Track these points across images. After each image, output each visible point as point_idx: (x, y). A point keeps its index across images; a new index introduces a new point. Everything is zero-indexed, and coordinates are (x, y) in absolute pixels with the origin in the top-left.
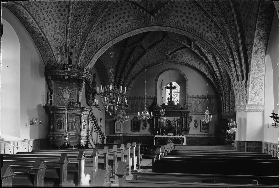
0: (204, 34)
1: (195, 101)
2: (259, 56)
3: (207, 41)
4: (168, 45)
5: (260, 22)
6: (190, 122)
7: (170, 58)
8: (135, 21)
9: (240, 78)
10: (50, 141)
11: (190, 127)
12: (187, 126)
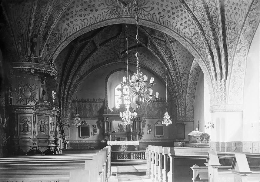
0: (181, 30)
2: (242, 54)
4: (121, 42)
5: (249, 18)
6: (144, 126)
7: (122, 57)
8: (106, 10)
9: (219, 77)
10: (49, 140)
11: (143, 131)
12: (140, 131)
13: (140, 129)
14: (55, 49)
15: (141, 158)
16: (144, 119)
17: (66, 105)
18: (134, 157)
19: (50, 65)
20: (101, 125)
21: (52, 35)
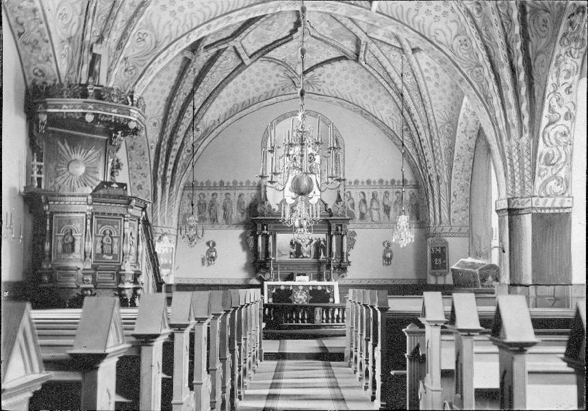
0: (427, 24)
1: (362, 195)
3: (435, 42)
13: (342, 253)
14: (144, 67)
15: (340, 321)
16: (352, 230)
17: (170, 195)
18: (323, 319)
19: (130, 103)
20: (251, 243)
21: (137, 37)
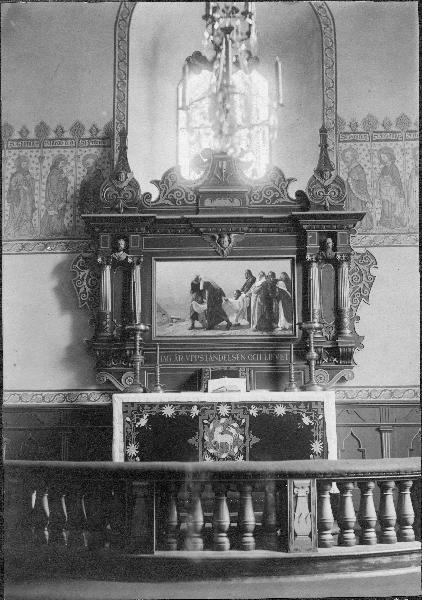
13: (338, 313)
15: (372, 534)
